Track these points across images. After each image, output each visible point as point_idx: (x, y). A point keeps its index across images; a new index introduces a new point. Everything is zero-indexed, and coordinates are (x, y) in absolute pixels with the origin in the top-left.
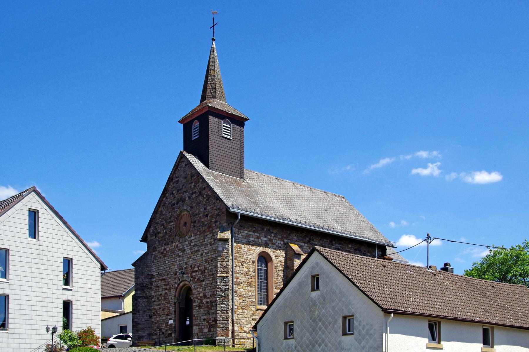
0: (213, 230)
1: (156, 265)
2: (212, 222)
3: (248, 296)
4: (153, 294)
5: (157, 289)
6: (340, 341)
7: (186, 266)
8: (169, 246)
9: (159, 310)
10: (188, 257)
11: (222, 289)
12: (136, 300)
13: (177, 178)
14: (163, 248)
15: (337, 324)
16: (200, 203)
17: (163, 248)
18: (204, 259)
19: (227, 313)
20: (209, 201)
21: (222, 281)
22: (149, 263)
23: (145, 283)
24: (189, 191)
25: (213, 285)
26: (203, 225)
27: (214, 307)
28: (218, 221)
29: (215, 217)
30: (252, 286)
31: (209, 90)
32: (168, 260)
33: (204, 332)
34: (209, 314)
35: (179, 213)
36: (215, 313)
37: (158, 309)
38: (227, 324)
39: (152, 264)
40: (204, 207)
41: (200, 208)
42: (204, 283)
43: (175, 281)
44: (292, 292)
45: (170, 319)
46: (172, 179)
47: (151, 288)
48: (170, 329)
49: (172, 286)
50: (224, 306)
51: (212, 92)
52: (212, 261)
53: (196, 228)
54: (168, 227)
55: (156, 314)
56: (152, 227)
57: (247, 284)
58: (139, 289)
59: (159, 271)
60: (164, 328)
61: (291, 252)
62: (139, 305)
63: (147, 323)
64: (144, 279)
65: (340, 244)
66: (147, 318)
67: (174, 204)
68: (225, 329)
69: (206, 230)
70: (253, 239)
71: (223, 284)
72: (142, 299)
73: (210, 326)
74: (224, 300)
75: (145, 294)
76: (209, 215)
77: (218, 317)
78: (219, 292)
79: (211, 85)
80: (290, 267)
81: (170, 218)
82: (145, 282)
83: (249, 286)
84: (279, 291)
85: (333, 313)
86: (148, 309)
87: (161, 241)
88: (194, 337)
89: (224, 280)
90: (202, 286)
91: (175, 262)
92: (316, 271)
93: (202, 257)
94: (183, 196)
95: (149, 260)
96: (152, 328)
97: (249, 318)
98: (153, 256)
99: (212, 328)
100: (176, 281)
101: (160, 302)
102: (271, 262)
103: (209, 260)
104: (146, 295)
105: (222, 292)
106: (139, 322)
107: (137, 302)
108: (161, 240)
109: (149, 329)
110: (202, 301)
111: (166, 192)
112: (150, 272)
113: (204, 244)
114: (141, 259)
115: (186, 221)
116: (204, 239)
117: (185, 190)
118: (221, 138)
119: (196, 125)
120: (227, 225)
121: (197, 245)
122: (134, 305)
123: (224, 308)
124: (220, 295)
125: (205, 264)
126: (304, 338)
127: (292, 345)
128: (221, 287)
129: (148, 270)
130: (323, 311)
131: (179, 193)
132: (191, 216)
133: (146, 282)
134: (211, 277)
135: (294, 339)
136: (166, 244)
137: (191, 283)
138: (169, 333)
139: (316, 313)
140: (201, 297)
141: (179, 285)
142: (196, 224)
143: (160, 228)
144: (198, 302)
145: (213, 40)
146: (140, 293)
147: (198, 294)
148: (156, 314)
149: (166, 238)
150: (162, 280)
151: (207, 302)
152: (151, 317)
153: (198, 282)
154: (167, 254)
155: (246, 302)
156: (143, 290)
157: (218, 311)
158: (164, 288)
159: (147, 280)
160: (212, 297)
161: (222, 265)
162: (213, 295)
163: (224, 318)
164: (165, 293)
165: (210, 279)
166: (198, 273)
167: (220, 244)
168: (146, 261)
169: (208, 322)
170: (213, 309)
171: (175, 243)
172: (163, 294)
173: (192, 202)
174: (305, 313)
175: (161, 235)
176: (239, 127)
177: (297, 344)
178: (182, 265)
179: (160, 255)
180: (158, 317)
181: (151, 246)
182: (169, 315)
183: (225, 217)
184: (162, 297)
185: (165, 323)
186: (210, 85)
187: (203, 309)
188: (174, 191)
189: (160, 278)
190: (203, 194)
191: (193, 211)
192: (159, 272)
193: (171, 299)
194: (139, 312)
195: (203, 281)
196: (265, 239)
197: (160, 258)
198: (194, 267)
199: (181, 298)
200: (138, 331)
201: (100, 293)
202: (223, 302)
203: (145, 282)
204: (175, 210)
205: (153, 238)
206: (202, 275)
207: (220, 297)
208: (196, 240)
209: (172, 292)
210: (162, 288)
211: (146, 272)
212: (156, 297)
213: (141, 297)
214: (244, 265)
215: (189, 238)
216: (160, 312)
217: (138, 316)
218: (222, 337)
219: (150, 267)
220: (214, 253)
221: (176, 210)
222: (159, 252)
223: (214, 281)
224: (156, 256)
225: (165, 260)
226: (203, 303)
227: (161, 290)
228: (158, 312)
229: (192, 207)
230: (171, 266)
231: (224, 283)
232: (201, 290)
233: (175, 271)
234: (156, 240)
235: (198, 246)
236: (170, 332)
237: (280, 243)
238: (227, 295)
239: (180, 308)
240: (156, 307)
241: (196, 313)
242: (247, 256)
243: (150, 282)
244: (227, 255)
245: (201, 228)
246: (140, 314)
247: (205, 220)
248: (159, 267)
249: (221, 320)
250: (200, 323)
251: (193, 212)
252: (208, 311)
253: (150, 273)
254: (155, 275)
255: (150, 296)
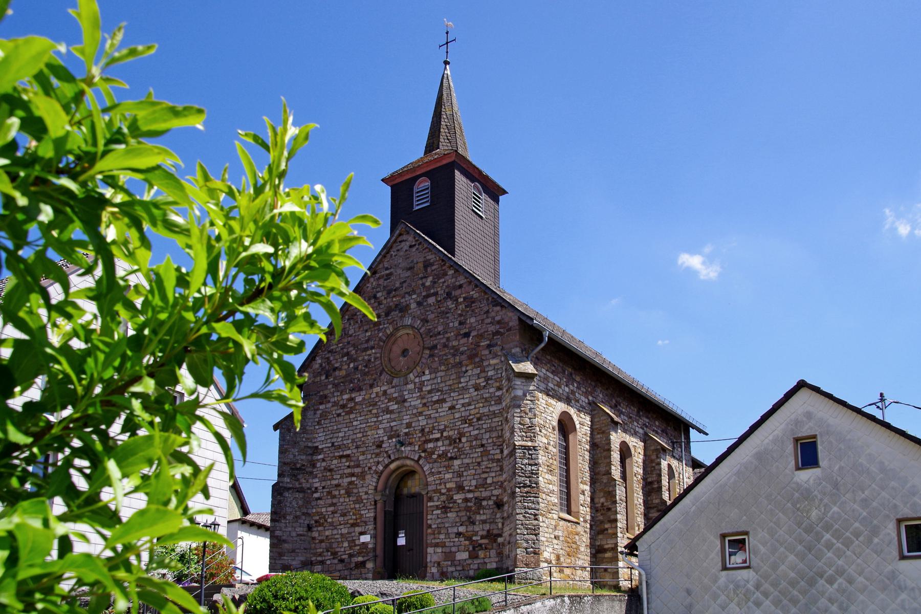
0: (482, 360)
2: (479, 346)
3: (549, 491)
5: (328, 474)
6: (893, 572)
8: (363, 393)
11: (526, 471)
12: (281, 494)
13: (387, 269)
14: (346, 397)
15: (881, 537)
16: (447, 313)
17: (346, 397)
18: (457, 415)
19: (536, 519)
20: (473, 308)
21: (524, 456)
22: (310, 424)
24: (418, 291)
25: (484, 467)
26: (456, 351)
27: (486, 509)
28: (497, 344)
29: (488, 336)
32: (359, 419)
34: (473, 523)
35: (391, 333)
36: (488, 521)
37: (330, 513)
39: (317, 427)
40: (459, 319)
42: (457, 463)
43: (376, 460)
44: (738, 473)
47: (311, 473)
48: (363, 552)
49: (370, 468)
51: (449, 138)
52: (479, 419)
53: (436, 359)
54: (360, 359)
55: (323, 523)
56: (317, 358)
57: (546, 467)
58: (286, 474)
59: (335, 440)
60: (345, 551)
62: (287, 504)
63: (301, 540)
64: (299, 455)
65: (647, 417)
68: (532, 552)
69: (464, 362)
70: (553, 386)
71: (526, 461)
72: (293, 492)
73: (474, 548)
74: (530, 493)
76: (473, 333)
78: (519, 476)
80: (600, 445)
85: (865, 514)
86: (304, 514)
88: (428, 568)
89: (529, 454)
91: (377, 423)
92: (806, 428)
95: (310, 419)
96: (312, 551)
97: (550, 533)
98: (319, 412)
99: (480, 550)
100: (381, 459)
101: (335, 501)
102: (573, 433)
104: (300, 486)
105: (526, 477)
106: (284, 538)
108: (342, 382)
109: (305, 553)
110: (452, 498)
112: (311, 442)
113: (458, 388)
115: (408, 348)
116: (460, 378)
117: (408, 290)
118: (470, 211)
121: (438, 391)
122: (276, 503)
123: (530, 509)
126: (783, 567)
127: (748, 581)
128: (523, 466)
130: (835, 509)
131: (391, 295)
132: (424, 336)
133: (302, 460)
134: (477, 450)
135: (751, 571)
136: (353, 389)
137: (421, 462)
139: (814, 514)
140: (449, 490)
141: (387, 466)
142: (436, 352)
145: (446, 63)
149: (354, 379)
150: (341, 457)
151: (466, 500)
152: (309, 528)
153: (439, 461)
154: (357, 407)
155: (546, 502)
156: (294, 475)
157: (518, 514)
158: (345, 472)
159: (304, 457)
160: (480, 490)
161: (524, 425)
162: (484, 485)
163: (530, 529)
165: (476, 455)
166: (440, 443)
169: (469, 538)
170: (484, 514)
171: (378, 386)
172: (342, 484)
174: (780, 514)
175: (343, 373)
177: (760, 578)
178: (398, 428)
179: (338, 410)
180: (328, 529)
181: (315, 394)
184: (340, 490)
186: (445, 127)
189: (337, 454)
190: (456, 296)
192: (333, 443)
193: (366, 493)
194: (285, 518)
195: (456, 458)
196: (567, 389)
197: (339, 415)
200: (281, 555)
201: (276, 463)
202: (527, 497)
204: (381, 327)
207: (522, 487)
208: (435, 381)
209: (367, 481)
210: (341, 472)
211: (302, 441)
212: (325, 490)
213: (290, 489)
214: (543, 431)
215: (416, 377)
216: (334, 520)
217: (284, 525)
219: (311, 434)
220: (486, 404)
221: (384, 327)
222: (335, 404)
223: (485, 459)
224: (326, 412)
226: (455, 502)
227: (338, 477)
229: (425, 321)
231: (529, 458)
232: (448, 476)
233: (377, 440)
235: (442, 391)
236: (360, 559)
237: (584, 400)
239: (385, 512)
241: (433, 521)
244: (532, 406)
245: (449, 358)
247: (463, 344)
250: (446, 540)
251: (429, 329)
252: (469, 518)
253: (310, 444)
254: (322, 449)
255: (308, 489)
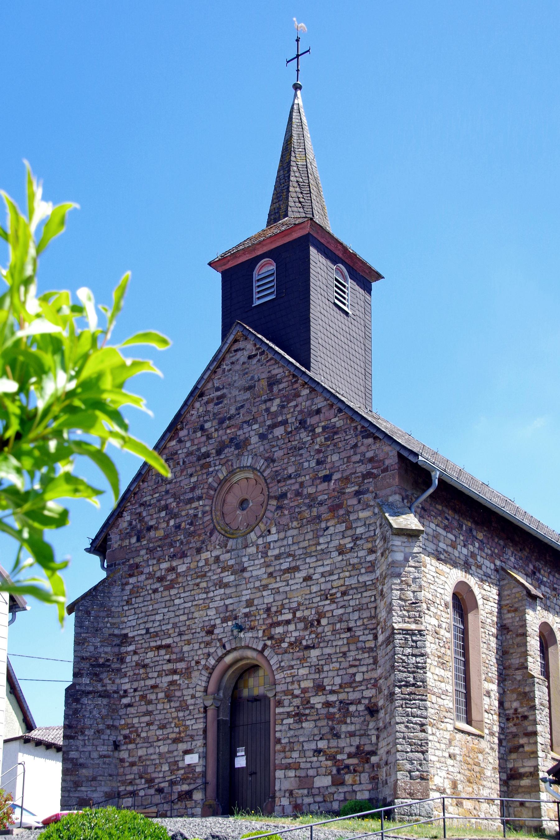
0: (348, 513)
1: (138, 611)
2: (344, 493)
4: (126, 687)
5: (142, 671)
7: (247, 610)
9: (145, 729)
10: (258, 587)
11: (408, 664)
12: (77, 701)
13: (218, 389)
14: (164, 566)
16: (300, 449)
17: (164, 566)
18: (315, 589)
19: (423, 731)
21: (406, 643)
23: (101, 658)
24: (260, 419)
25: (351, 659)
27: (354, 716)
30: (446, 667)
31: (294, 195)
32: (182, 595)
34: (337, 736)
38: (425, 762)
39: (126, 608)
40: (316, 457)
41: (301, 461)
42: (314, 653)
43: (206, 651)
45: (187, 752)
46: (202, 395)
47: (119, 670)
49: (198, 663)
50: (415, 710)
51: (302, 200)
52: (344, 594)
53: (286, 512)
55: (134, 740)
56: (125, 514)
59: (149, 625)
60: (164, 777)
61: (514, 591)
62: (85, 713)
63: (104, 763)
66: (104, 750)
67: (207, 455)
71: (409, 650)
73: (338, 771)
74: (415, 694)
75: (103, 686)
77: (397, 741)
78: (400, 671)
79: (299, 185)
80: (512, 628)
81: (193, 489)
82: (102, 655)
83: (441, 667)
86: (109, 727)
87: (158, 549)
88: (277, 799)
89: (413, 641)
90: (309, 660)
91: (207, 601)
93: (310, 586)
94: (240, 433)
95: (116, 597)
98: (128, 588)
99: (346, 773)
100: (212, 650)
101: (150, 708)
103: (334, 591)
104: (104, 688)
105: (409, 672)
106: (81, 761)
107: (79, 706)
110: (308, 702)
111: (179, 427)
113: (316, 551)
114: (94, 593)
119: (264, 270)
120: (401, 500)
121: (289, 555)
123: (414, 717)
124: (402, 681)
125: (320, 604)
128: (404, 658)
129: (111, 624)
131: (225, 425)
132: (268, 481)
133: (106, 653)
136: (174, 555)
137: (266, 653)
138: (182, 791)
142: (285, 502)
143: (155, 516)
144: (295, 704)
145: (297, 87)
146: (88, 682)
147: (293, 682)
148: (134, 740)
149: (175, 542)
150: (159, 648)
152: (116, 746)
153: (291, 651)
155: (436, 706)
157: (398, 723)
159: (108, 649)
160: (346, 690)
161: (405, 601)
164: (171, 682)
166: (291, 627)
167: (399, 543)
168: (108, 599)
170: (352, 723)
171: (208, 551)
172: (160, 685)
173: (273, 446)
175: (160, 533)
176: (363, 292)
178: (235, 608)
182: (182, 742)
183: (394, 479)
184: (157, 693)
185: (169, 763)
186: (296, 185)
187: (313, 722)
188: (206, 421)
189: (153, 644)
191: (279, 468)
194: (83, 733)
195: (313, 647)
196: (465, 551)
197: (155, 591)
198: (279, 612)
199: (221, 694)
202: (410, 700)
203: (102, 655)
204: (211, 469)
205: (130, 543)
206: (307, 632)
208: (285, 542)
210: (158, 668)
211: (106, 627)
212: (137, 693)
213: (89, 693)
214: (432, 609)
215: (258, 537)
216: (150, 734)
218: (411, 800)
221: (215, 470)
223: (352, 647)
225: (170, 596)
227: (156, 675)
228: (143, 735)
230: (193, 613)
231: (412, 647)
234: (141, 545)
235: (294, 556)
238: (421, 681)
239: (218, 721)
240: (136, 720)
241: (284, 733)
242: (436, 588)
243: (118, 655)
244: (416, 575)
246: (87, 738)
248: (148, 616)
249: (408, 750)
250: (300, 760)
251: (276, 471)
253: (116, 632)
255: (116, 692)
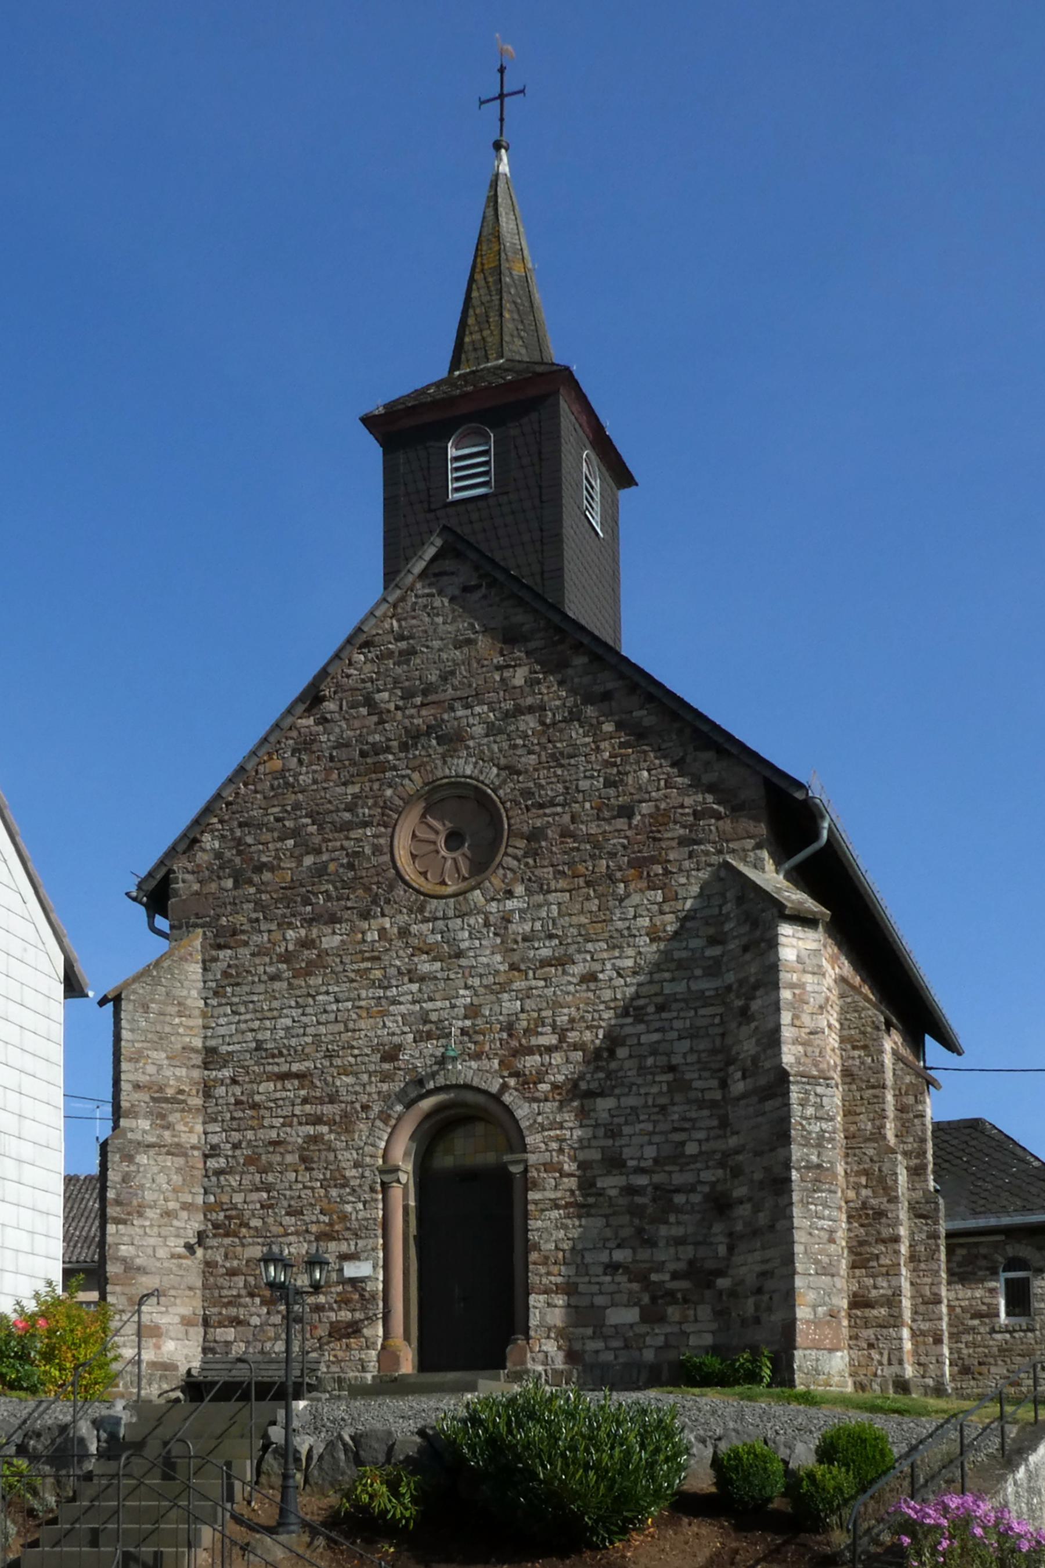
11: (810, 1133)
33: (608, 1323)
84: (108, 1195)
106: (138, 1262)
107: (133, 1168)
133: (178, 1079)
159: (182, 1072)
169: (642, 1278)
194: (140, 1215)
195: (602, 1094)
217: (141, 1231)
246: (147, 1223)
249: (812, 1272)
